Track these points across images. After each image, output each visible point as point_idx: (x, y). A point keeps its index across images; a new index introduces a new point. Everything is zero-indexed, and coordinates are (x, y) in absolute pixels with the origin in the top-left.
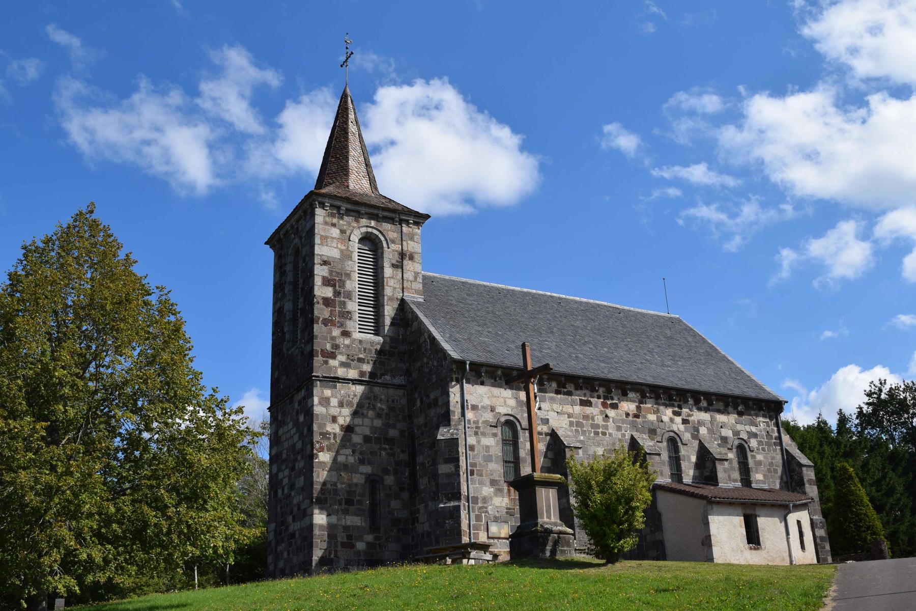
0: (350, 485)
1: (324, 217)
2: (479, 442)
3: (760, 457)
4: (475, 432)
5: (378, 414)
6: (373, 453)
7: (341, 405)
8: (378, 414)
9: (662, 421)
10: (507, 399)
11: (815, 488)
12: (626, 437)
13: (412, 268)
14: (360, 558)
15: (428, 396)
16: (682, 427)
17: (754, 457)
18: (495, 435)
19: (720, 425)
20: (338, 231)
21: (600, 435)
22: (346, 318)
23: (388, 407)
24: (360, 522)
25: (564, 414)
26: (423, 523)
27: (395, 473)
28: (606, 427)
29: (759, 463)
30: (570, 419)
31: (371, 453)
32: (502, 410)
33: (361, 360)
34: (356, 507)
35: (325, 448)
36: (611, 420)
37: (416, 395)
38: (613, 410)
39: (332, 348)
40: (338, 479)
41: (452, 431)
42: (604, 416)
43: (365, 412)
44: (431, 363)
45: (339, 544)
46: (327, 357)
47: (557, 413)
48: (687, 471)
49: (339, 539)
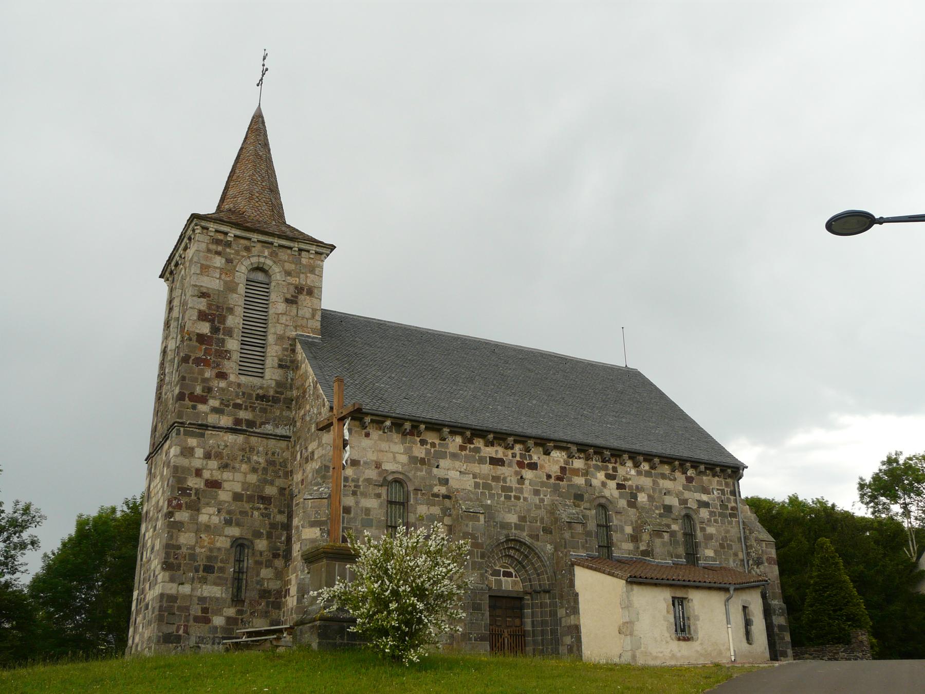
0: (211, 550)
1: (207, 243)
2: (357, 503)
3: (711, 530)
4: (353, 491)
5: (254, 468)
6: (244, 513)
7: (208, 456)
8: (254, 468)
9: (591, 485)
10: (397, 455)
11: (776, 568)
12: (545, 503)
13: (310, 304)
14: (216, 635)
15: (306, 448)
16: (616, 493)
17: (703, 529)
18: (378, 496)
19: (664, 491)
20: (223, 261)
21: (513, 499)
22: (224, 358)
23: (267, 461)
24: (220, 592)
25: (469, 474)
26: (293, 597)
27: (269, 536)
28: (521, 491)
29: (709, 537)
30: (476, 480)
31: (241, 513)
32: (389, 466)
33: (238, 406)
34: (216, 575)
35: (184, 505)
36: (527, 482)
37: (298, 448)
38: (530, 471)
39: (203, 391)
40: (197, 542)
41: (323, 489)
42: (519, 477)
43: (237, 465)
44: (312, 410)
45: (191, 618)
46: (196, 402)
47: (460, 472)
48: (619, 543)
49: (192, 612)
